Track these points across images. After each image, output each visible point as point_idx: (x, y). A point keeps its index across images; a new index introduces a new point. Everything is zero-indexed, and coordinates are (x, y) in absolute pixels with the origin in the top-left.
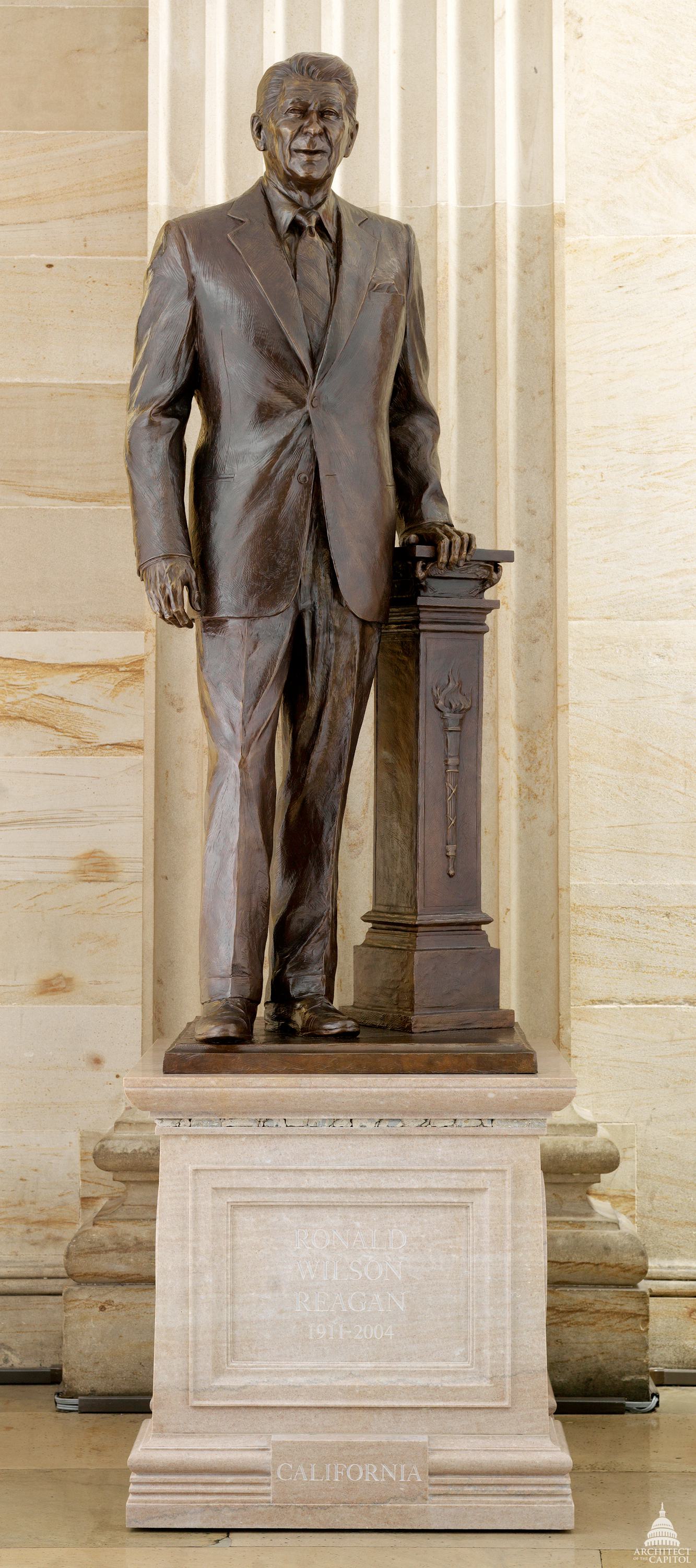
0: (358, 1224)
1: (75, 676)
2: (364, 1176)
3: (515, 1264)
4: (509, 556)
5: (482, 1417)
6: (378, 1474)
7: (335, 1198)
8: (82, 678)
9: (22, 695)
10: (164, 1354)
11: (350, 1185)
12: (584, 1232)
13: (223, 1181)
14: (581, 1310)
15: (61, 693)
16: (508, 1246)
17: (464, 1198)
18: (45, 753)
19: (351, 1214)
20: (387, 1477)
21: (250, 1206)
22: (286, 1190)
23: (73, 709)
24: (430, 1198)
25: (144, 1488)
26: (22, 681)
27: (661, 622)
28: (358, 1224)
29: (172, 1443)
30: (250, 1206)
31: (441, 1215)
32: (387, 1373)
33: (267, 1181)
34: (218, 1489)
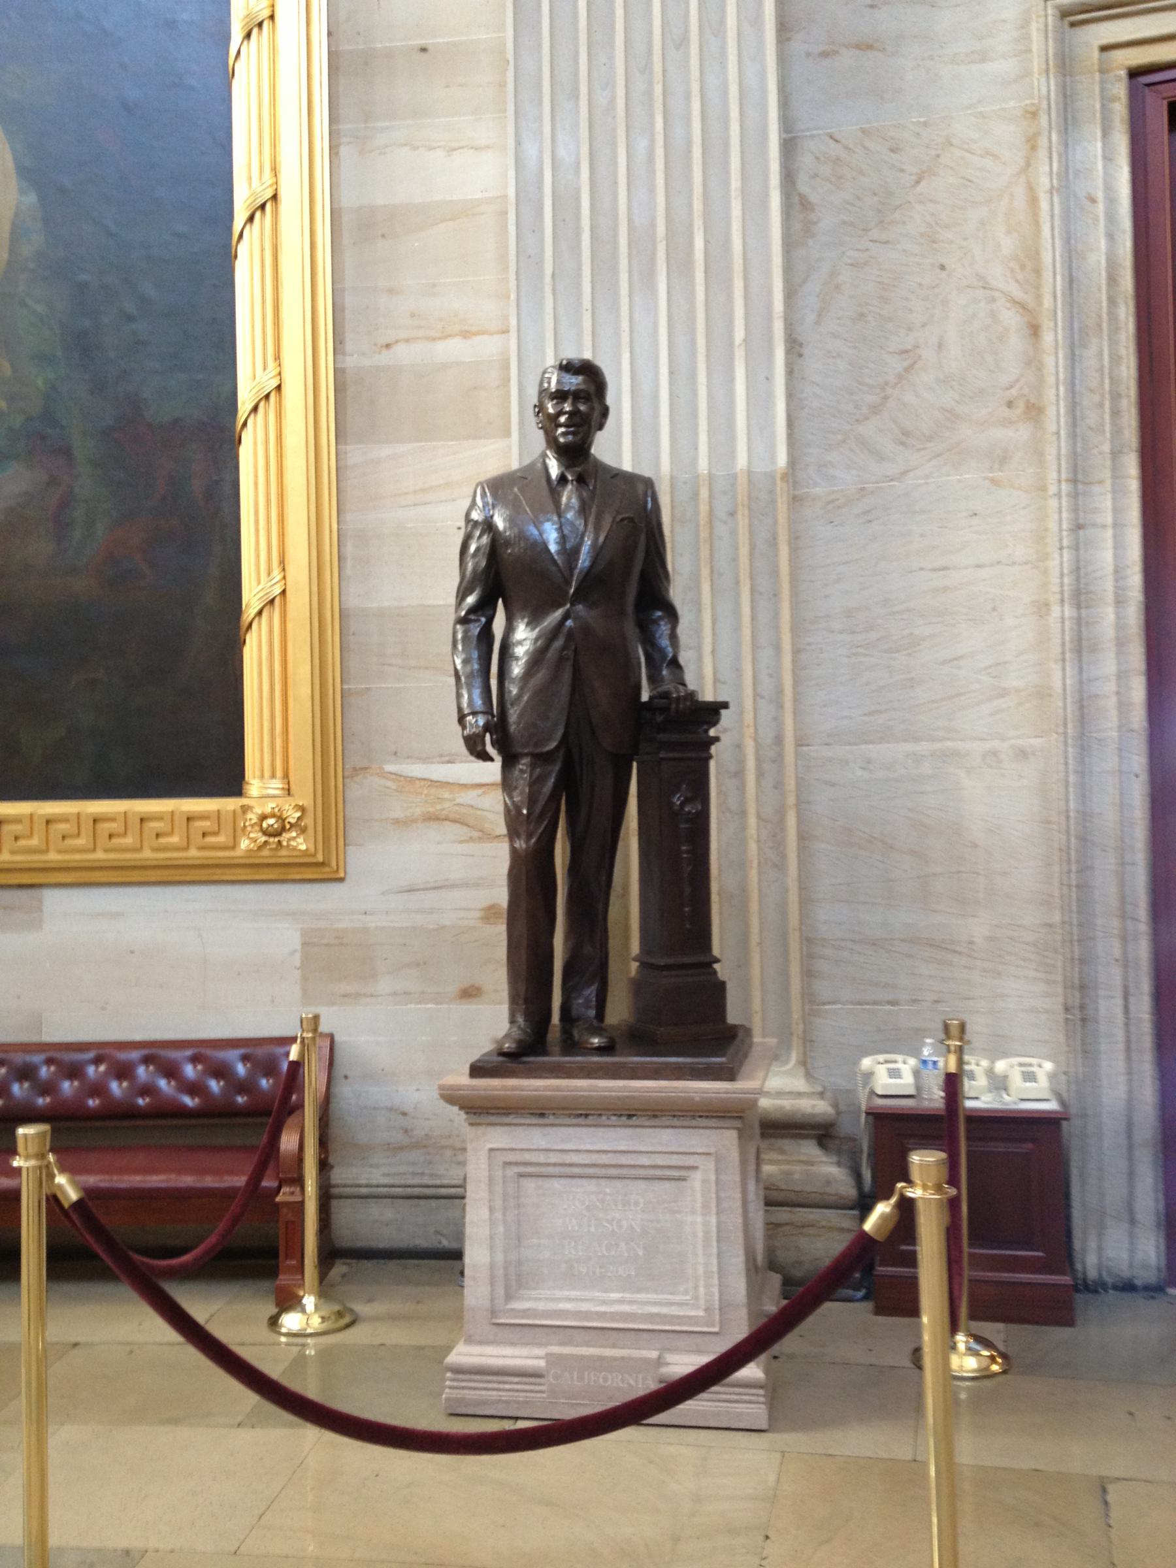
0: (608, 1190)
1: (480, 791)
2: (610, 1155)
3: (719, 1224)
4: (725, 705)
5: (699, 1339)
6: (623, 1381)
7: (591, 1171)
8: (484, 793)
9: (447, 805)
10: (472, 1283)
11: (600, 1162)
12: (814, 1168)
13: (511, 1157)
14: (812, 1226)
15: (470, 802)
16: (714, 1210)
17: (683, 1173)
18: (461, 842)
19: (603, 1182)
20: (630, 1385)
21: (530, 1175)
22: (555, 1165)
23: (479, 813)
24: (658, 1172)
25: (455, 1384)
26: (446, 795)
27: (863, 746)
28: (608, 1190)
29: (477, 1349)
30: (530, 1175)
31: (667, 1185)
32: (631, 1302)
33: (541, 1158)
34: (507, 1386)
